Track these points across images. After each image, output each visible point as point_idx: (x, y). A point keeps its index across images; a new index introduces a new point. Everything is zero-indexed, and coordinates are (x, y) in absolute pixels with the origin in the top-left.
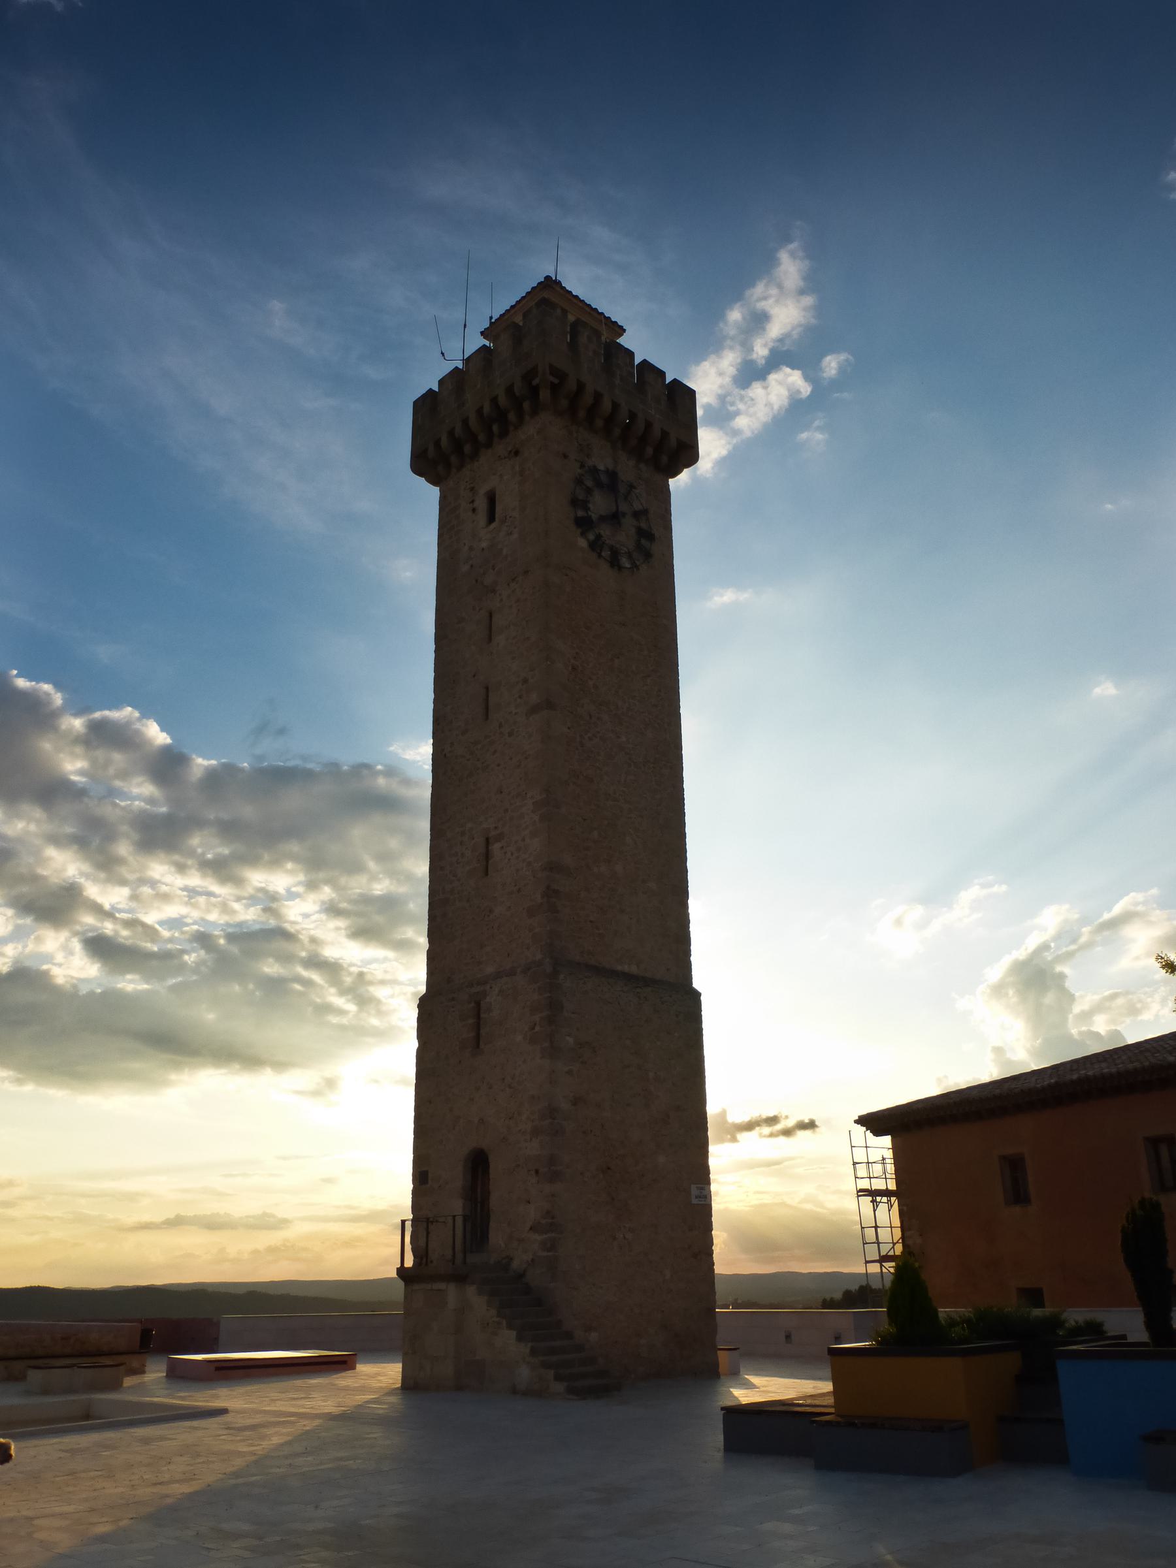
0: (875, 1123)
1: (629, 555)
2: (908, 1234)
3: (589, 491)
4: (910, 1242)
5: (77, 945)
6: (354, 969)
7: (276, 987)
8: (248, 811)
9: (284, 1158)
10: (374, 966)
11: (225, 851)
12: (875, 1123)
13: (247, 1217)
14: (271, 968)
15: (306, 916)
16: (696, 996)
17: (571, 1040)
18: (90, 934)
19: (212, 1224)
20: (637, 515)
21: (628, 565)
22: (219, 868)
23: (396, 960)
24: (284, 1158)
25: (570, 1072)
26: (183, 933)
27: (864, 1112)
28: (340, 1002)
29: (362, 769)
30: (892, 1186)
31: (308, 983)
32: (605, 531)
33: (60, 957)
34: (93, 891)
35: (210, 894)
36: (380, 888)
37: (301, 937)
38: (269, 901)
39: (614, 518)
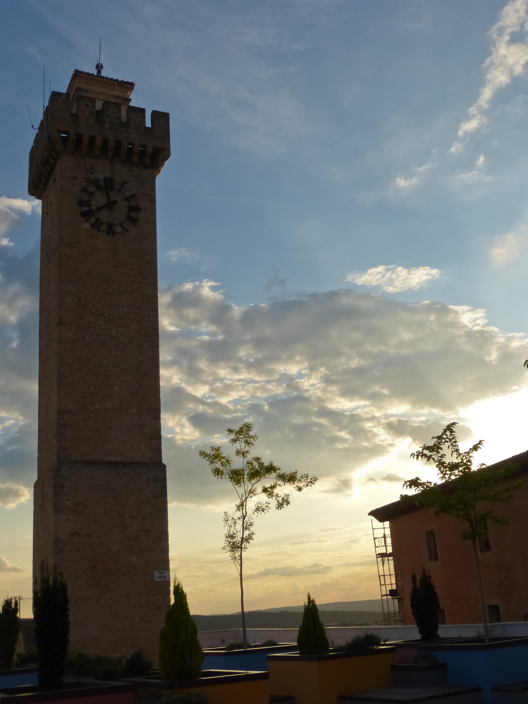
0: (380, 514)
1: (121, 224)
2: (398, 578)
3: (92, 194)
4: (398, 584)
5: (184, 421)
6: (348, 413)
7: (302, 430)
8: (268, 331)
9: (324, 531)
10: (359, 410)
11: (260, 356)
12: (380, 514)
13: (305, 567)
14: (297, 420)
15: (313, 385)
16: (164, 467)
17: (69, 503)
18: (192, 414)
19: (287, 573)
20: (127, 199)
21: (120, 230)
22: (256, 366)
23: (372, 406)
24: (324, 531)
25: (69, 520)
26: (242, 406)
27: (374, 508)
28: (343, 434)
29: (333, 294)
30: (390, 550)
31: (320, 425)
32: (104, 216)
33: (178, 429)
34: (189, 389)
35: (255, 382)
36: (355, 363)
37: (312, 399)
38: (289, 381)
39: (110, 205)
